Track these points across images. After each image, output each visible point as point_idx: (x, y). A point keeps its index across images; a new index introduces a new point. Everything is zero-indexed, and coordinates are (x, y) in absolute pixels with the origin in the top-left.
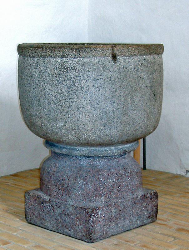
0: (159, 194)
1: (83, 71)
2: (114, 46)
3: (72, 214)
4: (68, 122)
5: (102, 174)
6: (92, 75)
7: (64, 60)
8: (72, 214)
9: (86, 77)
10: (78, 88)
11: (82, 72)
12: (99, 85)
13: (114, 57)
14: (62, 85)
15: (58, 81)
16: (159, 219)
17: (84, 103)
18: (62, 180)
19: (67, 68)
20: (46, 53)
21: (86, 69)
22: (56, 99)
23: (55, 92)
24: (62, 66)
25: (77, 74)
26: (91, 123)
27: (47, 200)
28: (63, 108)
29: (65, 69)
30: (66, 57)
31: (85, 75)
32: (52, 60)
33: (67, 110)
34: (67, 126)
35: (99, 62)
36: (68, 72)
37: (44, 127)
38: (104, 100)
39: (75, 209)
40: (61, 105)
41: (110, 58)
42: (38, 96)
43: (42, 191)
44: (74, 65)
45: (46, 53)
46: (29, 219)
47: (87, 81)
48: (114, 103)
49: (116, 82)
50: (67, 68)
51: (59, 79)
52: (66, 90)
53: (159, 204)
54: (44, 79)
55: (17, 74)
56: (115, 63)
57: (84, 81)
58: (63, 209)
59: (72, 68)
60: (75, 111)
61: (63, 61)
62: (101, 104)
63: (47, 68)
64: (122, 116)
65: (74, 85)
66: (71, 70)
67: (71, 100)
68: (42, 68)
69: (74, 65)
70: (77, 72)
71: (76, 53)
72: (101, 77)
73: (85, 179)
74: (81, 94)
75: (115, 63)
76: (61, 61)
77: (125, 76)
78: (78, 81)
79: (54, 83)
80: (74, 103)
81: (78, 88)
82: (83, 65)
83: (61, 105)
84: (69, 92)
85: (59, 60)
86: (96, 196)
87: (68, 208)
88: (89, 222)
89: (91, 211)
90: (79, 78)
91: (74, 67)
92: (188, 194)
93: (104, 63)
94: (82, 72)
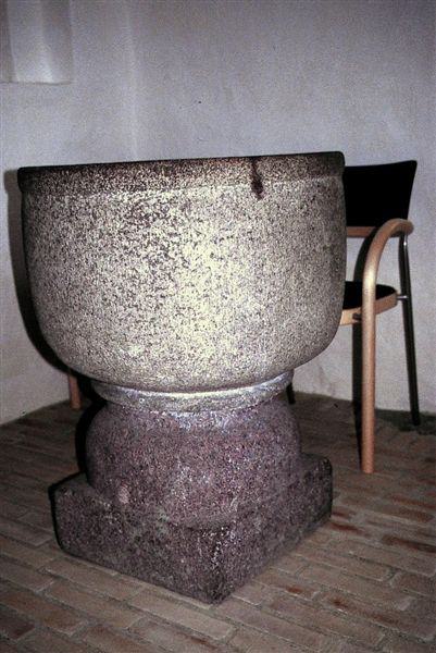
0: (333, 464)
1: (186, 221)
2: (254, 160)
3: (168, 542)
4: (156, 343)
5: (229, 449)
6: (210, 229)
7: (138, 196)
8: (168, 542)
9: (195, 235)
10: (175, 263)
11: (183, 224)
12: (226, 251)
13: (257, 187)
14: (135, 258)
15: (126, 248)
16: (335, 514)
17: (188, 296)
18: (141, 467)
19: (147, 216)
20: (91, 181)
21: (192, 215)
22: (123, 292)
23: (118, 276)
24: (132, 210)
25: (171, 230)
26: (211, 342)
27: (106, 509)
28: (140, 312)
29: (141, 218)
30: (142, 190)
31: (191, 231)
32: (108, 198)
33: (151, 315)
34: (154, 354)
35: (222, 196)
36: (148, 226)
37: (95, 357)
38: (240, 286)
39: (176, 531)
40: (136, 306)
41: (248, 186)
42: (77, 287)
43: (90, 485)
44: (164, 206)
45: (91, 181)
46: (67, 544)
47: (196, 244)
48: (261, 291)
49: (264, 242)
50: (147, 216)
51: (127, 244)
52: (147, 268)
53: (334, 482)
54: (90, 244)
55: (432, 338)
56: (260, 198)
57: (190, 245)
58: (145, 530)
59: (158, 214)
60: (171, 318)
61: (136, 200)
62: (232, 296)
63: (95, 218)
64: (278, 319)
65: (166, 255)
66: (158, 220)
67: (159, 292)
68: (84, 219)
69: (164, 206)
70: (173, 225)
71: (167, 179)
72: (229, 233)
73: (192, 465)
74: (183, 276)
75: (260, 198)
76: (130, 199)
77: (283, 228)
78: (175, 246)
79: (116, 252)
80: (168, 300)
81: (175, 263)
82: (186, 205)
83: (136, 306)
84: (153, 272)
85: (124, 197)
86: (220, 499)
87: (157, 529)
88: (210, 561)
89: (214, 538)
90: (176, 239)
91: (165, 212)
92: (434, 488)
93: (235, 198)
94: (183, 224)
